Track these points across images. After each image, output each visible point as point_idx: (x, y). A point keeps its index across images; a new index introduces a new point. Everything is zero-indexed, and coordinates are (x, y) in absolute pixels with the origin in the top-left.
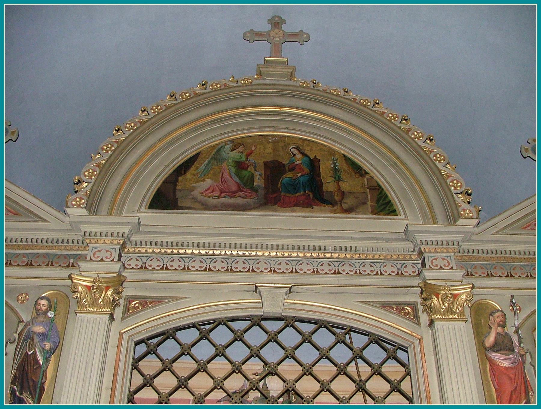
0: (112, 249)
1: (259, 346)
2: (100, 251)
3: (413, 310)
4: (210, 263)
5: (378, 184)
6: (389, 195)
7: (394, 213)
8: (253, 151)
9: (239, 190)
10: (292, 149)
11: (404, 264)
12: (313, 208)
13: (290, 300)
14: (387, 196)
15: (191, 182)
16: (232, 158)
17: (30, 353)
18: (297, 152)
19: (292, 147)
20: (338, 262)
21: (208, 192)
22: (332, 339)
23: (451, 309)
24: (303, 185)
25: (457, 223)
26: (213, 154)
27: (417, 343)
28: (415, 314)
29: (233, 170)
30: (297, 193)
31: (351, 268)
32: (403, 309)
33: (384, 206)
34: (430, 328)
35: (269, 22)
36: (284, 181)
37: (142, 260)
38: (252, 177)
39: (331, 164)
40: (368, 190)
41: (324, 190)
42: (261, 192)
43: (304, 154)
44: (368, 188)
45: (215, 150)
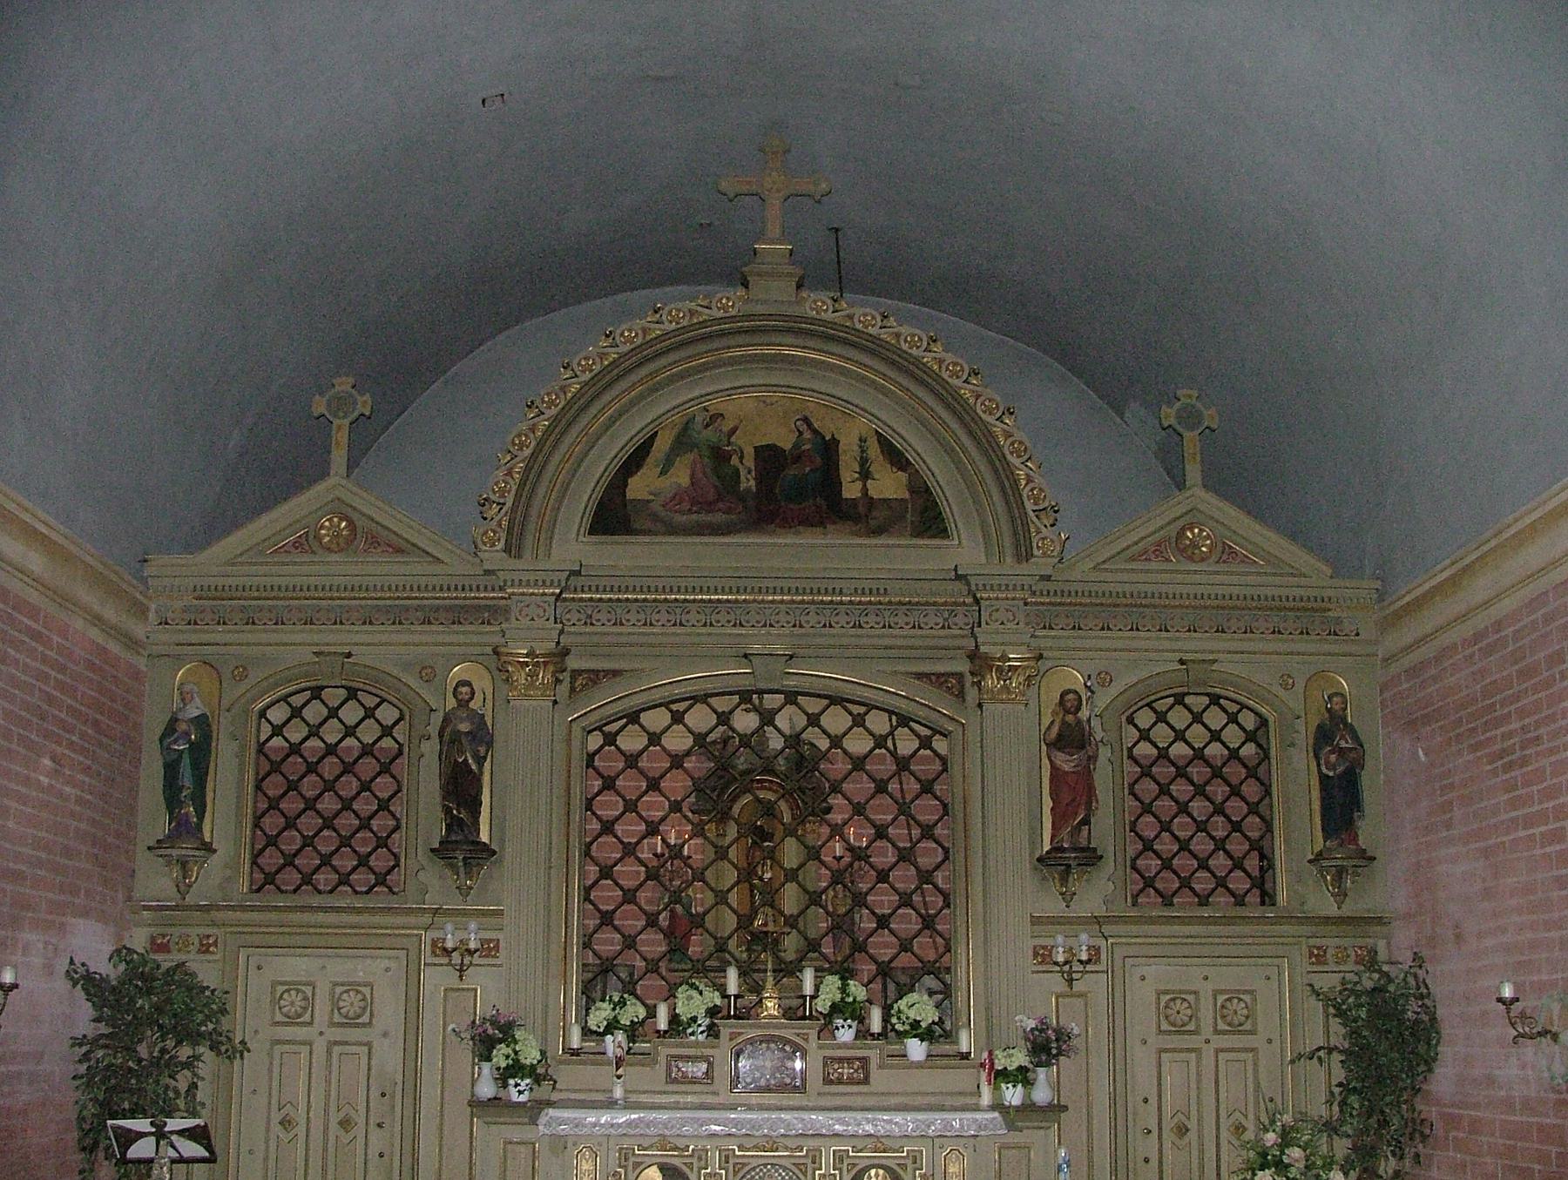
9: (720, 498)
11: (953, 611)
17: (460, 760)
31: (879, 619)
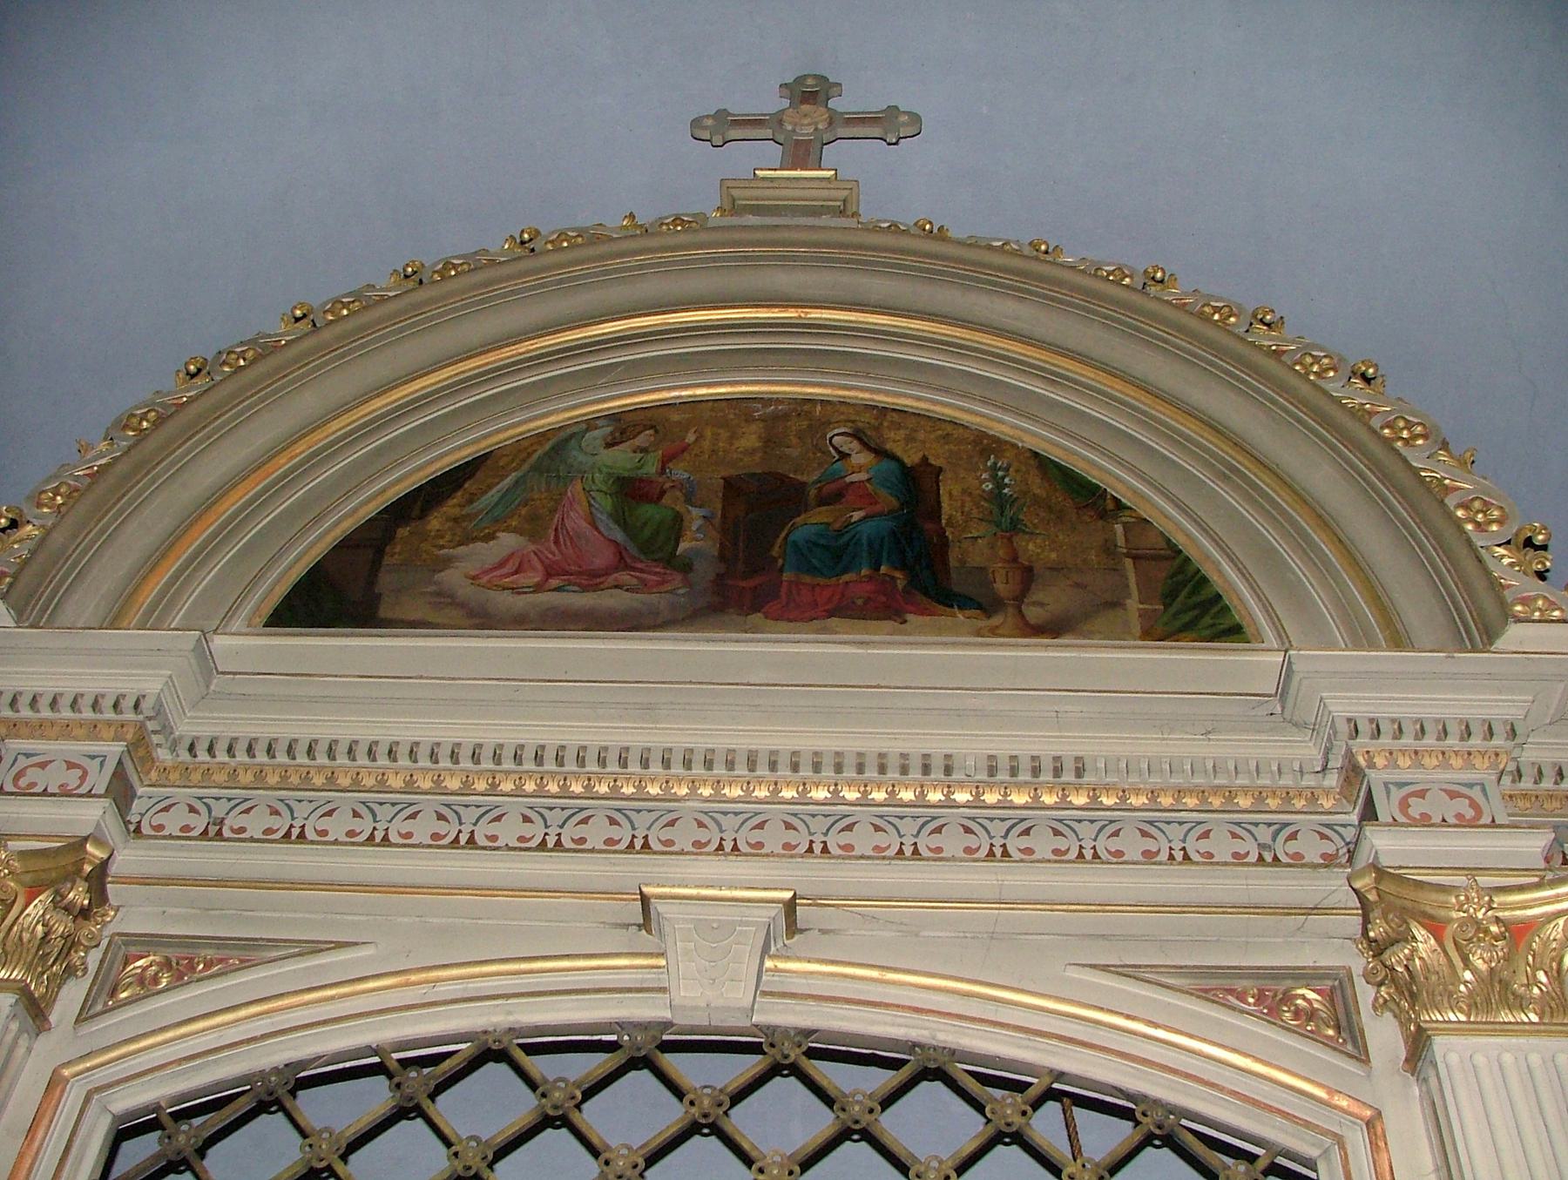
0: (93, 757)
1: (642, 1147)
2: (43, 765)
3: (1332, 1000)
4: (478, 821)
5: (1168, 541)
6: (1213, 577)
7: (1241, 636)
8: (689, 445)
9: (622, 561)
10: (836, 438)
12: (905, 622)
13: (788, 958)
14: (1204, 581)
15: (441, 542)
16: (607, 467)
18: (855, 445)
19: (836, 431)
20: (1003, 820)
21: (498, 573)
22: (968, 1128)
23: (1505, 985)
24: (870, 545)
25: (1499, 644)
26: (535, 456)
27: (1358, 1140)
28: (1342, 1017)
29: (606, 503)
30: (845, 571)
32: (1287, 998)
33: (1196, 612)
34: (1412, 1079)
35: (786, 92)
36: (797, 536)
37: (210, 812)
38: (677, 526)
39: (985, 480)
40: (1128, 562)
41: (953, 563)
42: (705, 571)
43: (880, 453)
44: (1127, 555)
45: (547, 446)
